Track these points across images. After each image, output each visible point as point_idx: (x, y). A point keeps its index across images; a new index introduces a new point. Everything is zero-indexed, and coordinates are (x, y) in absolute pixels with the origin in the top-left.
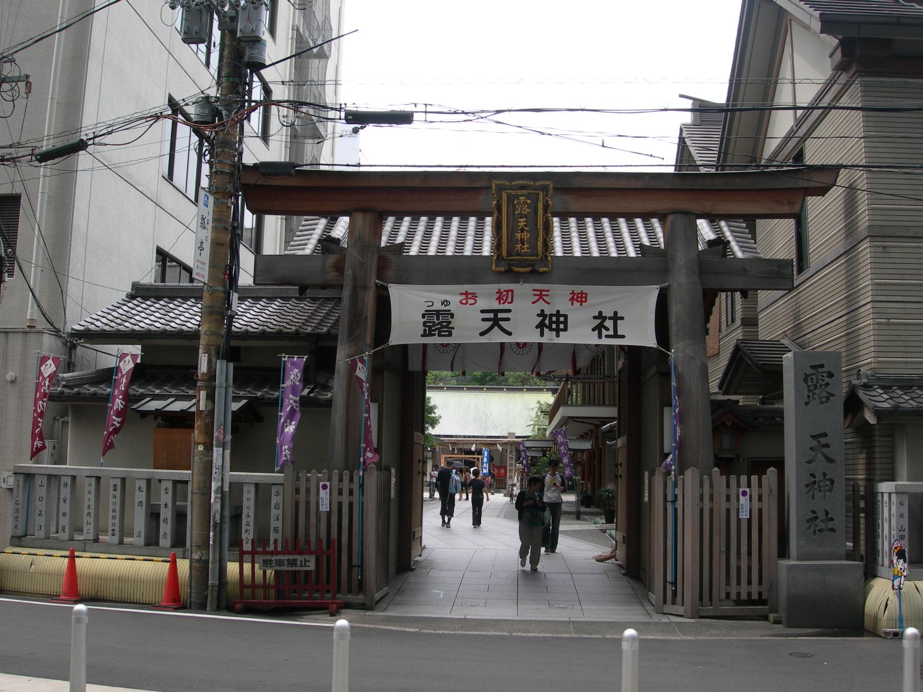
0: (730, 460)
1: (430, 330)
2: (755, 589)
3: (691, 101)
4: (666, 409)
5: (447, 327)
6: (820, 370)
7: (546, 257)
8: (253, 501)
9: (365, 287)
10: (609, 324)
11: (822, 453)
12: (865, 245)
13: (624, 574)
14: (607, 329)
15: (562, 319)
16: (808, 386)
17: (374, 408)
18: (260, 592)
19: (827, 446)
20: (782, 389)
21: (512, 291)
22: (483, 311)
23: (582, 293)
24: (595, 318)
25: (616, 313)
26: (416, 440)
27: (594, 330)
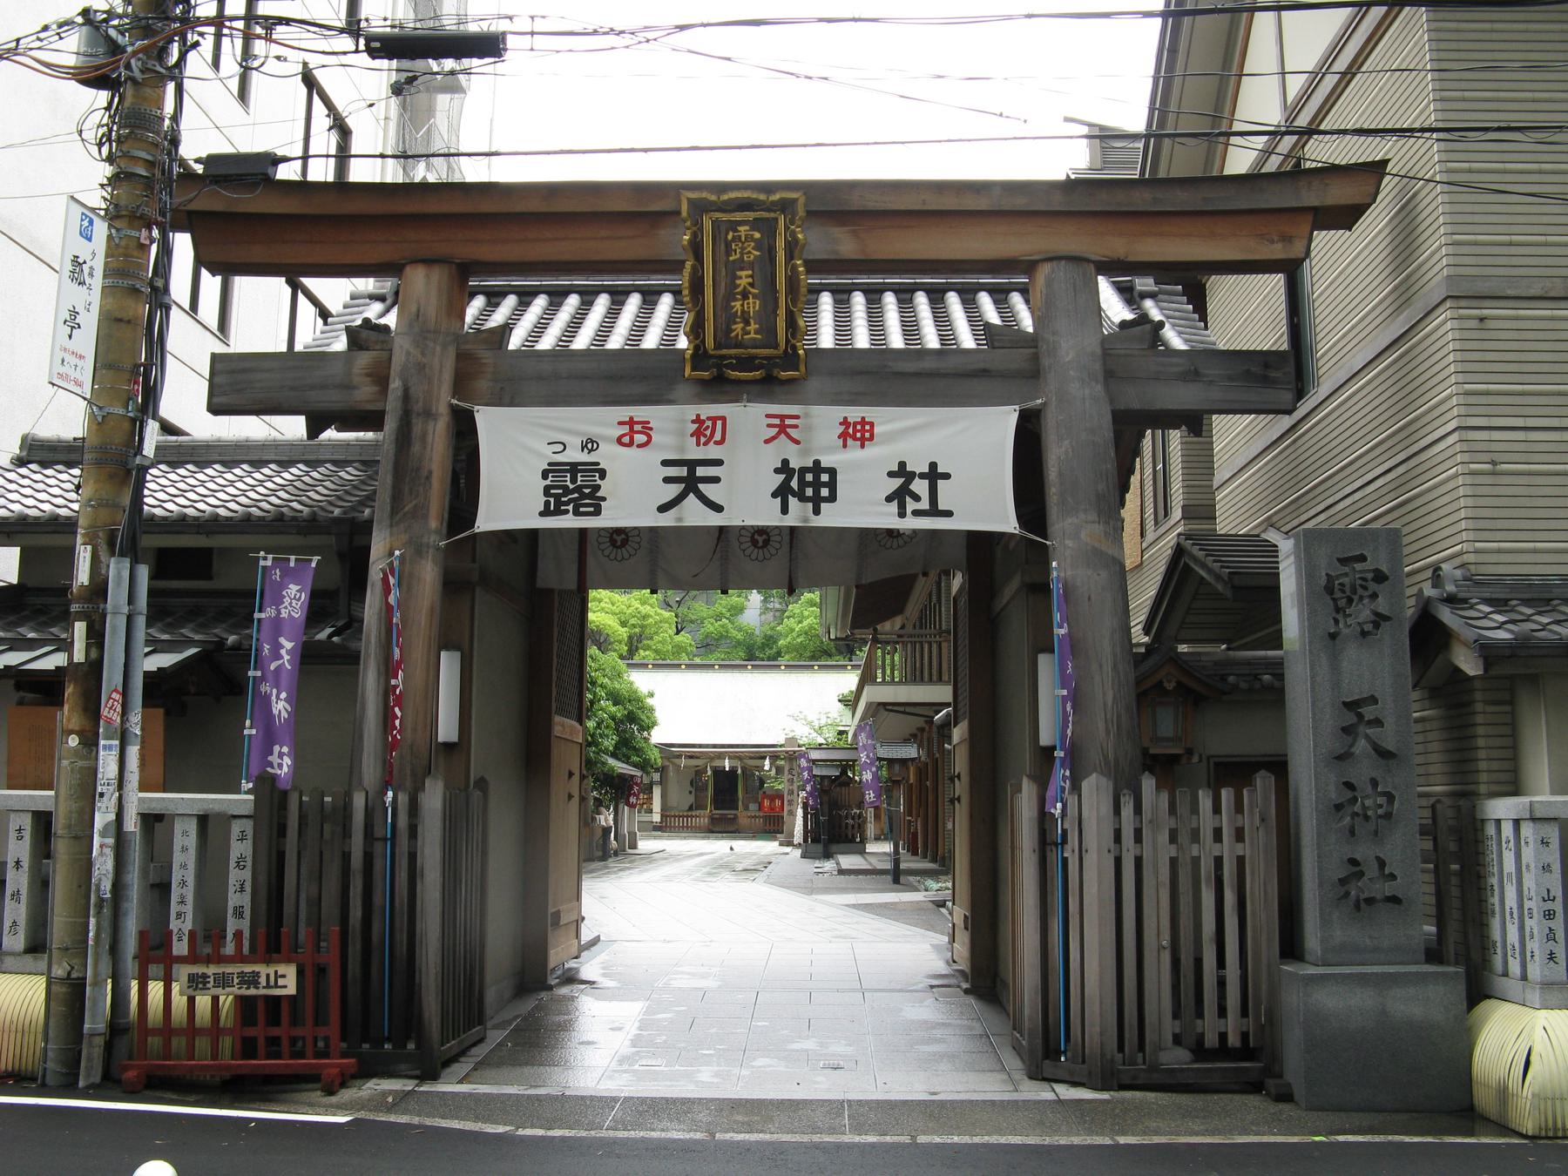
0: (1174, 759)
1: (558, 503)
2: (1233, 1026)
4: (1043, 659)
5: (592, 496)
6: (1358, 566)
7: (794, 348)
8: (192, 852)
9: (428, 414)
10: (920, 487)
11: (1367, 737)
12: (1442, 315)
13: (966, 992)
14: (917, 498)
15: (825, 478)
16: (1334, 600)
17: (449, 664)
18: (202, 1044)
19: (1378, 722)
20: (1280, 621)
21: (723, 419)
22: (665, 463)
23: (863, 422)
24: (891, 474)
25: (933, 466)
26: (557, 730)
27: (889, 499)
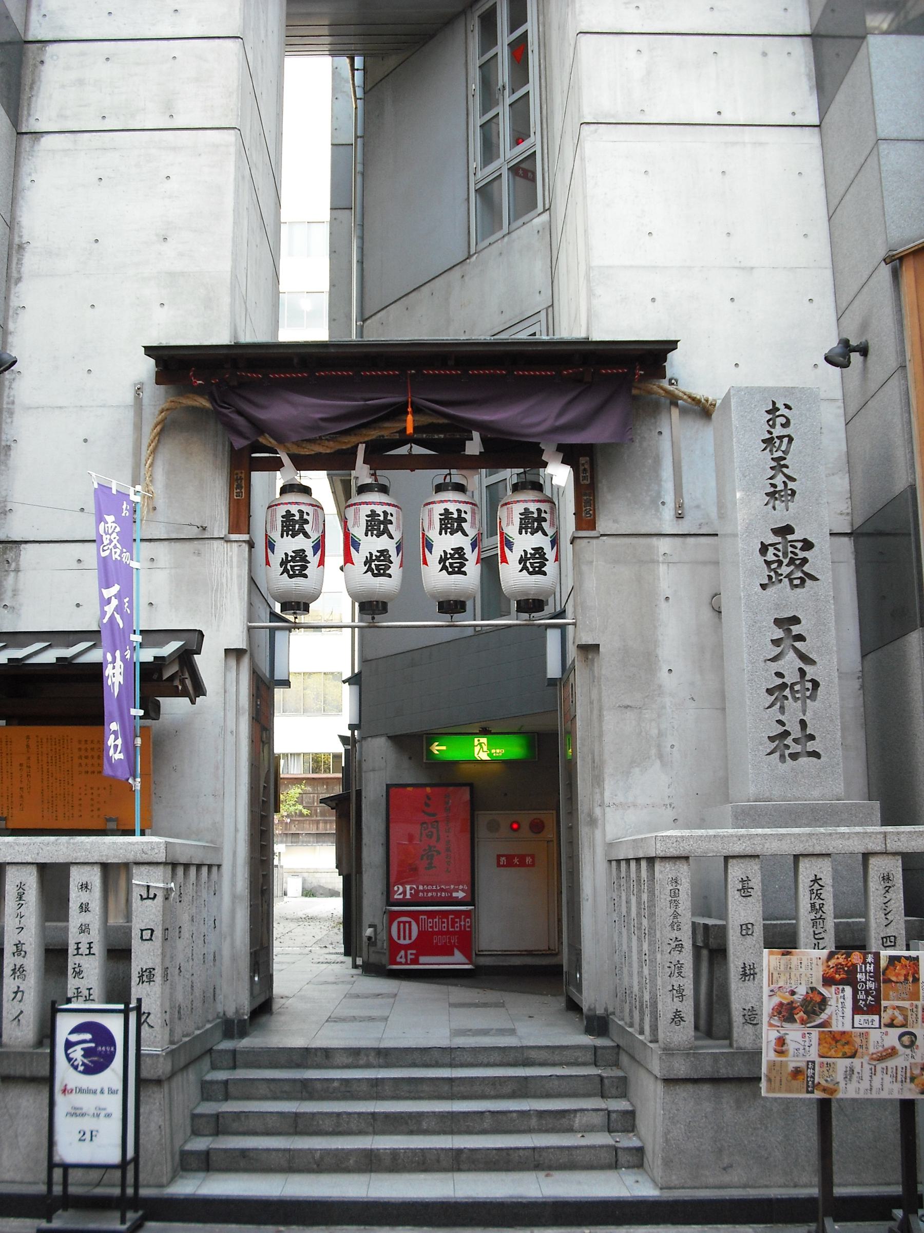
3: (48, 1074)
11: (796, 650)
